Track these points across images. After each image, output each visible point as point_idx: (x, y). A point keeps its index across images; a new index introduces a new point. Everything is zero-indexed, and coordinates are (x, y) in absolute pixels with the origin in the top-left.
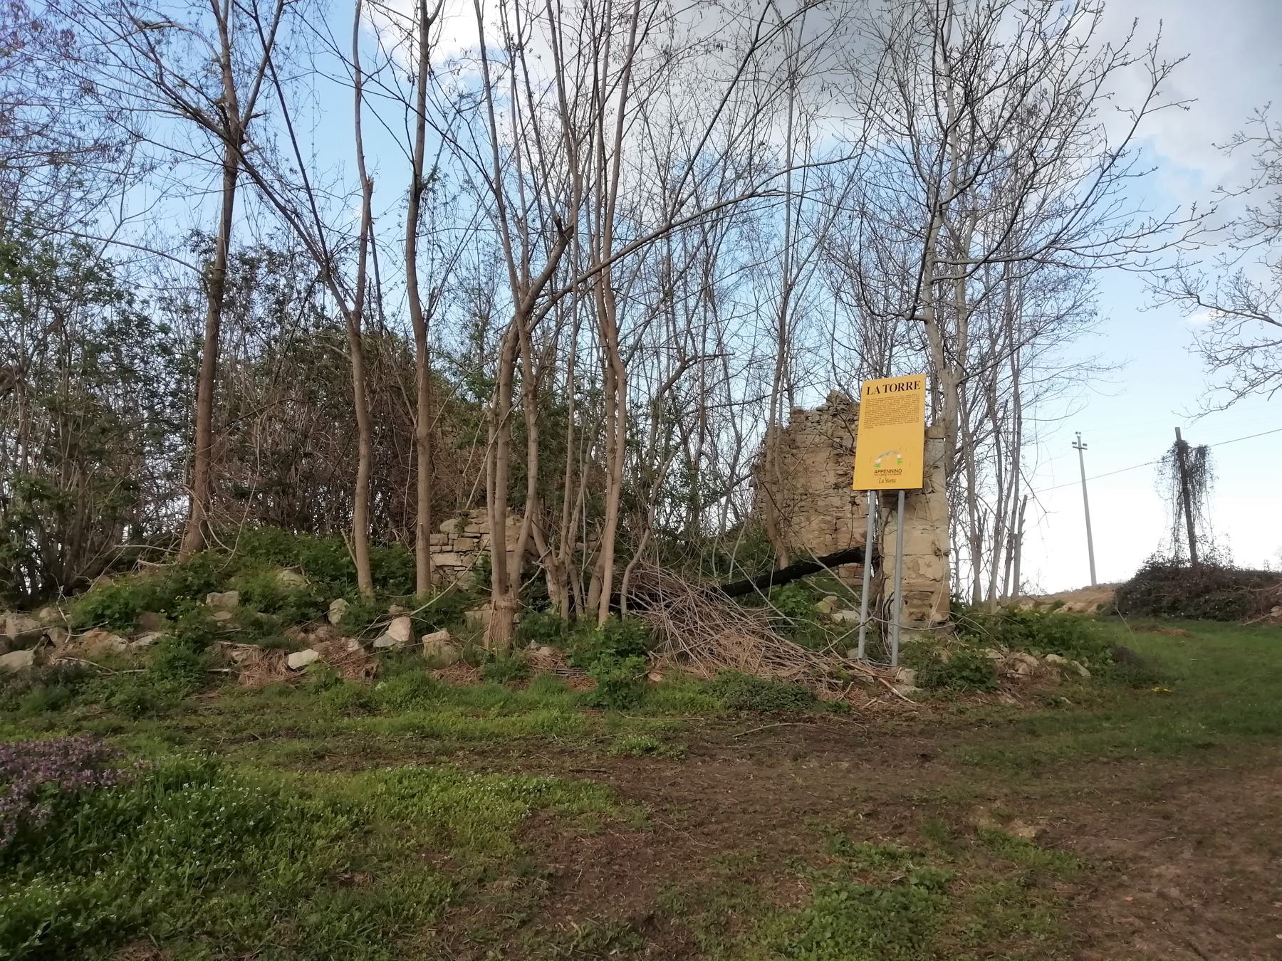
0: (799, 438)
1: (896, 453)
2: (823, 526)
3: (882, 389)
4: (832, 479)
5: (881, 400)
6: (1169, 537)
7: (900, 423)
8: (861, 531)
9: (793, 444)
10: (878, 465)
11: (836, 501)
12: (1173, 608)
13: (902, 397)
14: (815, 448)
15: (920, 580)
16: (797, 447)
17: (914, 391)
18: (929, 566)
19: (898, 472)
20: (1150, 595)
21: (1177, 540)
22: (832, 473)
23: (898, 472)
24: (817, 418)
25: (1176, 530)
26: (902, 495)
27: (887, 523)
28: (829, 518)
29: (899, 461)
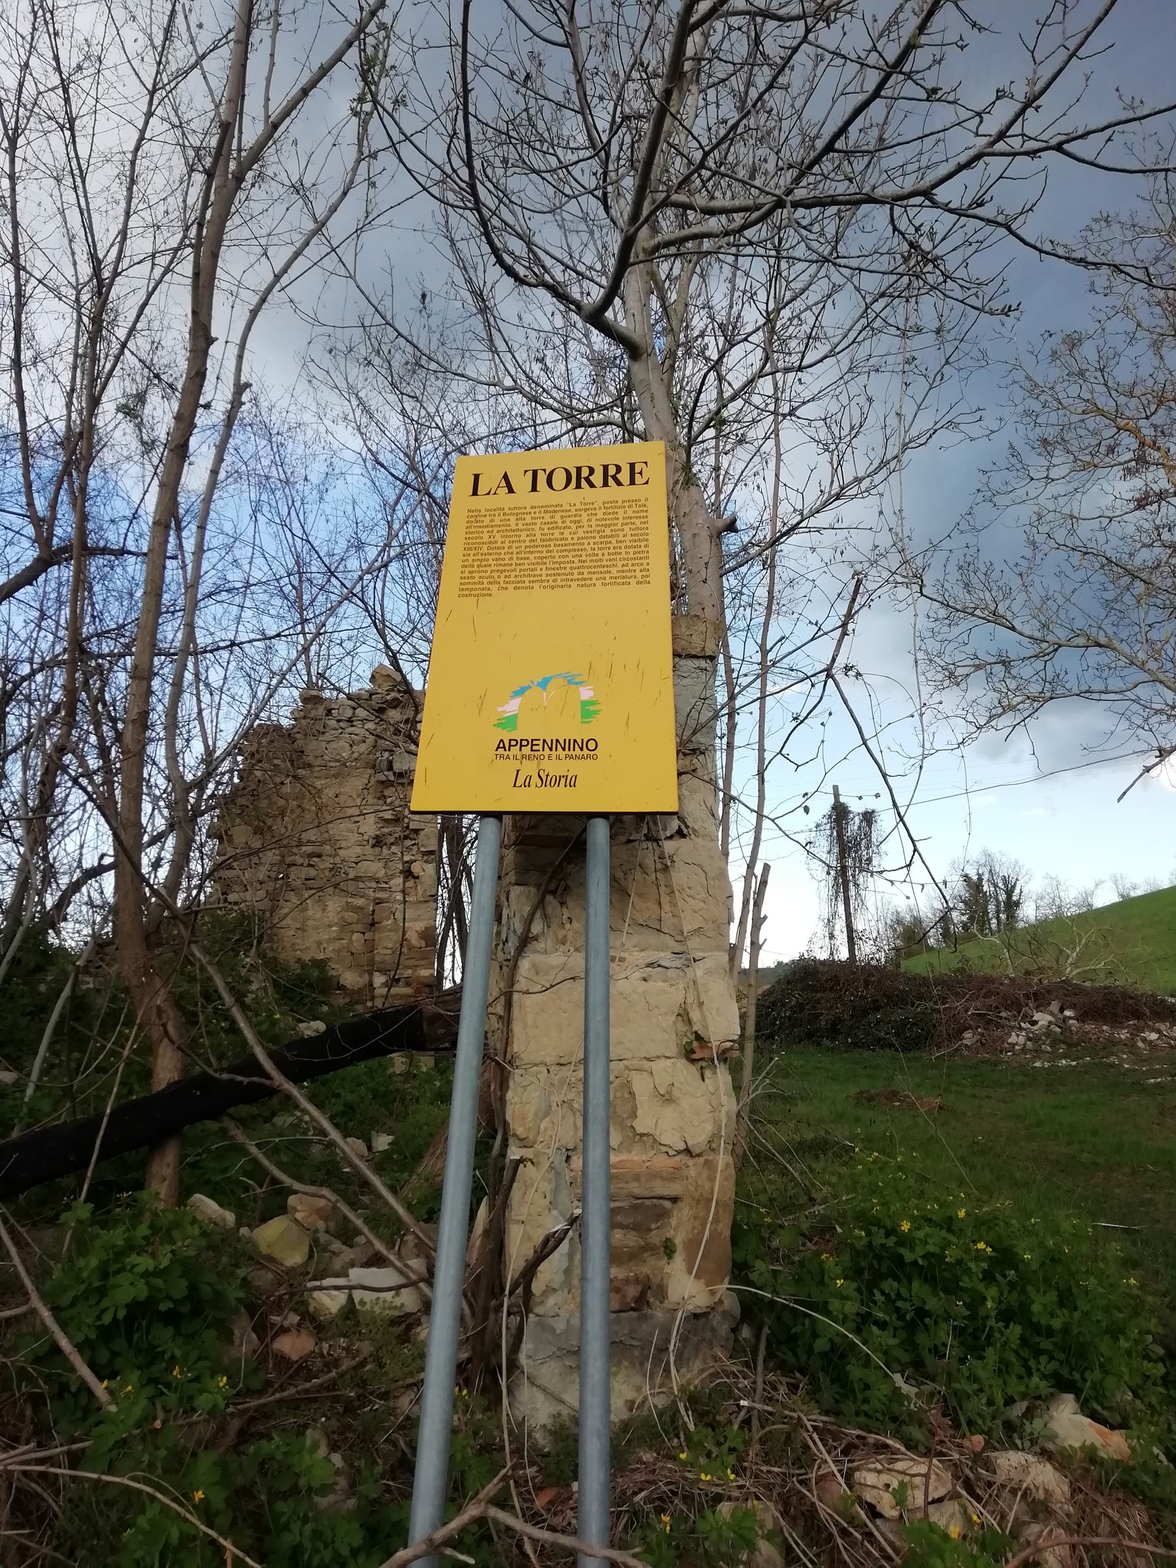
0: (313, 747)
1: (572, 681)
2: (351, 916)
3: (522, 483)
4: (370, 827)
5: (519, 512)
6: (822, 931)
7: (584, 583)
8: (420, 926)
9: (298, 757)
10: (509, 722)
11: (375, 868)
12: (833, 1030)
13: (588, 507)
14: (342, 770)
15: (637, 1156)
16: (309, 766)
17: (627, 492)
18: (667, 1098)
19: (585, 748)
20: (802, 1010)
21: (832, 936)
22: (371, 819)
23: (585, 748)
24: (349, 713)
25: (830, 923)
26: (600, 833)
27: (526, 941)
28: (360, 902)
29: (588, 711)
